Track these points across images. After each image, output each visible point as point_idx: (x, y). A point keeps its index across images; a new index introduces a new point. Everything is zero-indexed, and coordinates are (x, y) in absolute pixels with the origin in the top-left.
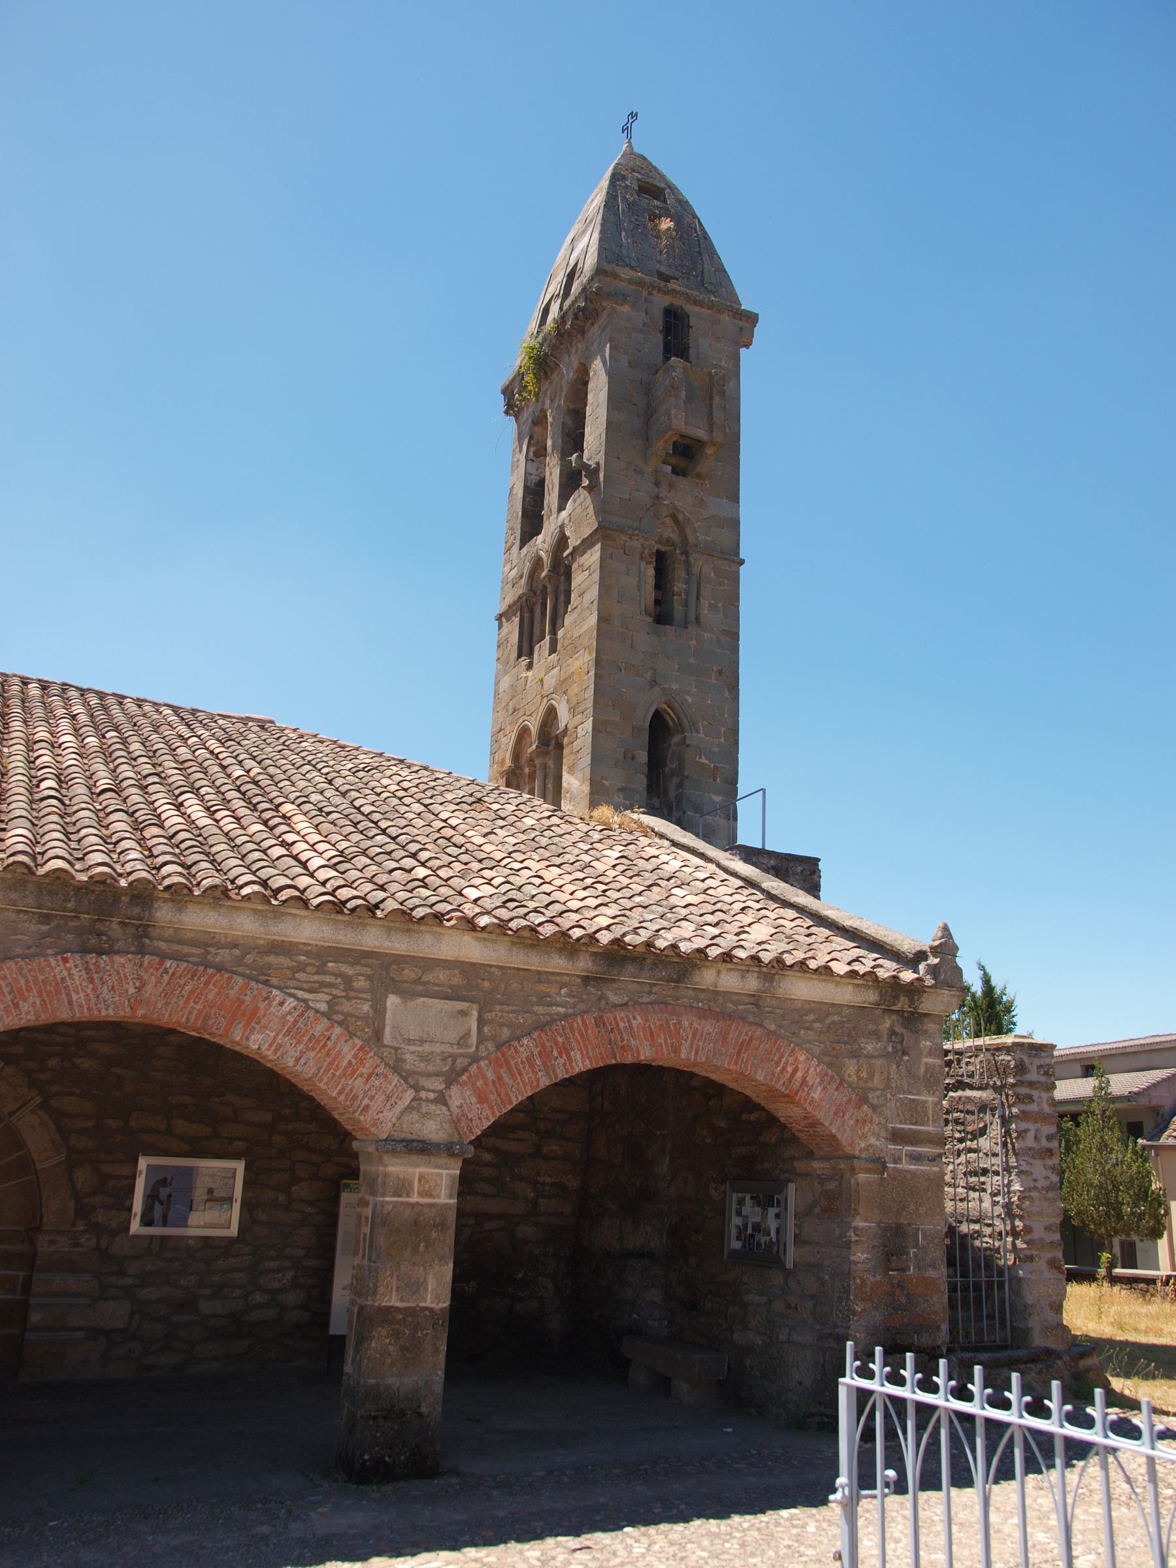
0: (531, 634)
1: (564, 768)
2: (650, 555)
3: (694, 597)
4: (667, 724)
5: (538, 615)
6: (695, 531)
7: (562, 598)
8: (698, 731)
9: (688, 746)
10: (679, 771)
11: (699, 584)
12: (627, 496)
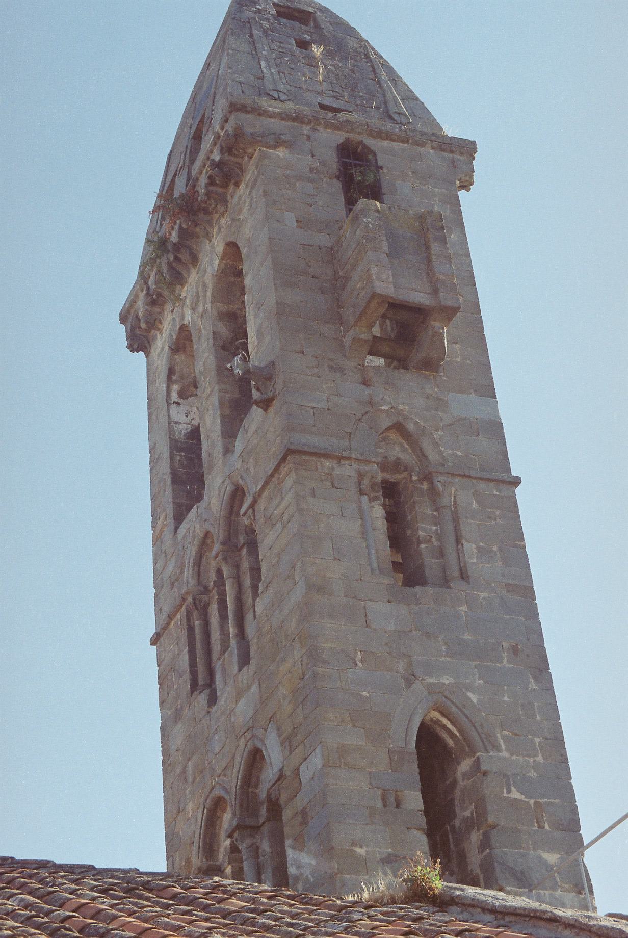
0: (208, 651)
1: (288, 842)
2: (373, 486)
3: (452, 539)
4: (445, 746)
5: (214, 620)
6: (436, 444)
7: (247, 581)
8: (499, 750)
9: (485, 774)
10: (478, 820)
11: (456, 520)
12: (323, 405)
